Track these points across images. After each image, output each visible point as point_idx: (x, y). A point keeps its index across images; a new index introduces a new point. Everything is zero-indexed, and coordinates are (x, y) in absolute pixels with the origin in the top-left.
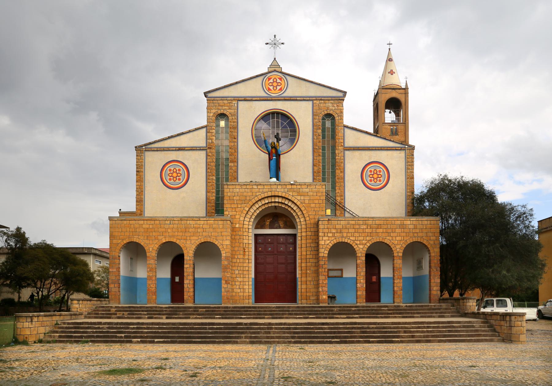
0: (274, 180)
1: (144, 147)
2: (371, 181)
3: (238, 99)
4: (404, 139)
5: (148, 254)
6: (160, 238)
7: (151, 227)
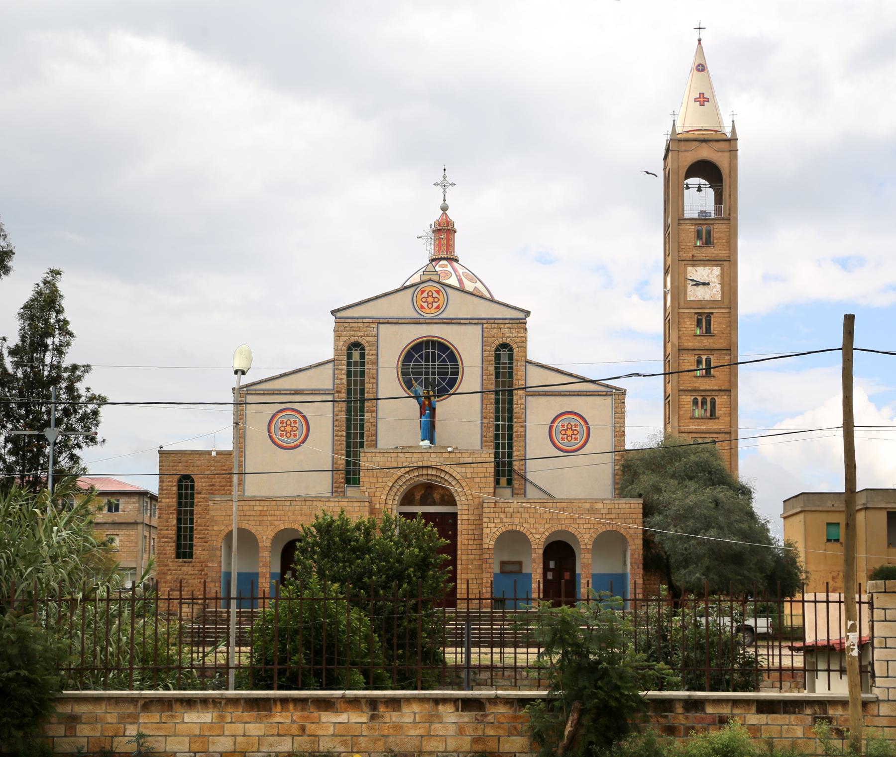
0: (427, 443)
1: (245, 389)
2: (563, 439)
3: (378, 321)
4: (727, 255)
5: (261, 545)
6: (276, 523)
7: (265, 509)
